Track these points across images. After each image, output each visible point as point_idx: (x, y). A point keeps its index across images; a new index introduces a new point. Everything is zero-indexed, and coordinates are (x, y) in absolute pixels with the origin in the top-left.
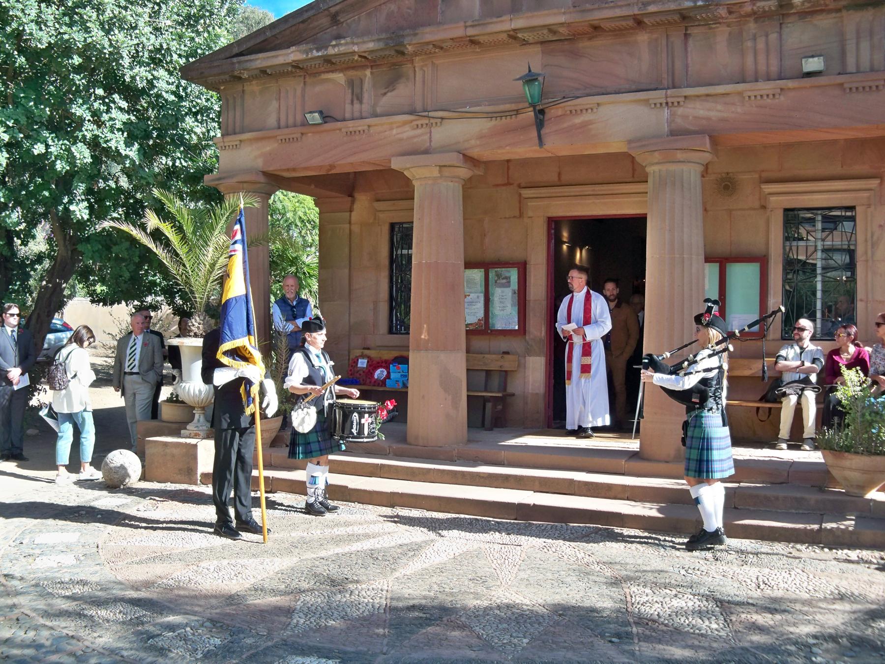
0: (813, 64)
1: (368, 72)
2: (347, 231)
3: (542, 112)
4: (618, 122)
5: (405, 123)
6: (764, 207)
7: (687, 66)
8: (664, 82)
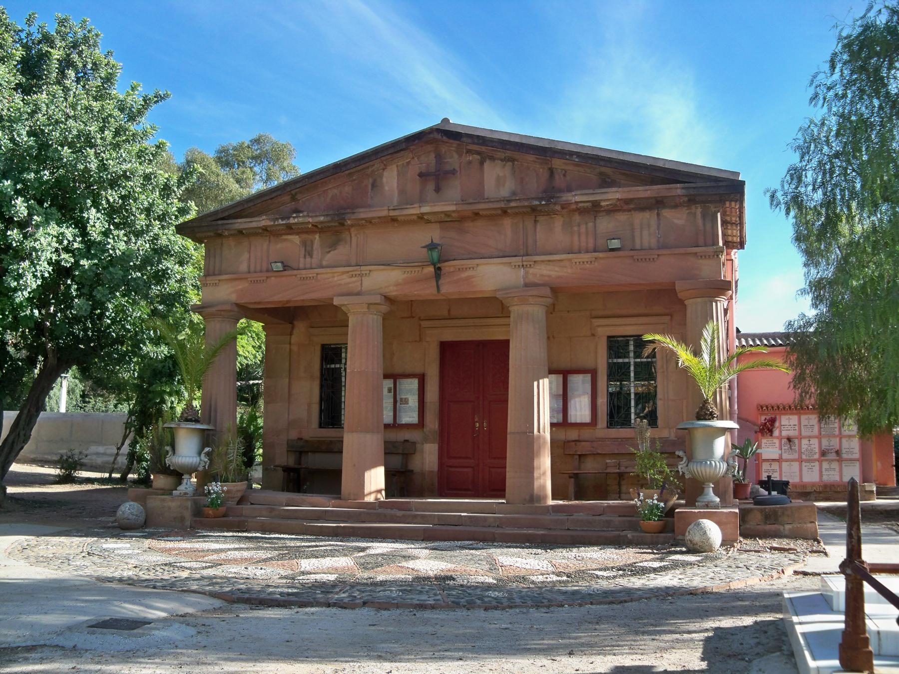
0: (615, 244)
1: (317, 236)
2: (288, 350)
3: (439, 269)
4: (492, 275)
5: (343, 273)
6: (593, 335)
7: (535, 241)
8: (522, 252)
